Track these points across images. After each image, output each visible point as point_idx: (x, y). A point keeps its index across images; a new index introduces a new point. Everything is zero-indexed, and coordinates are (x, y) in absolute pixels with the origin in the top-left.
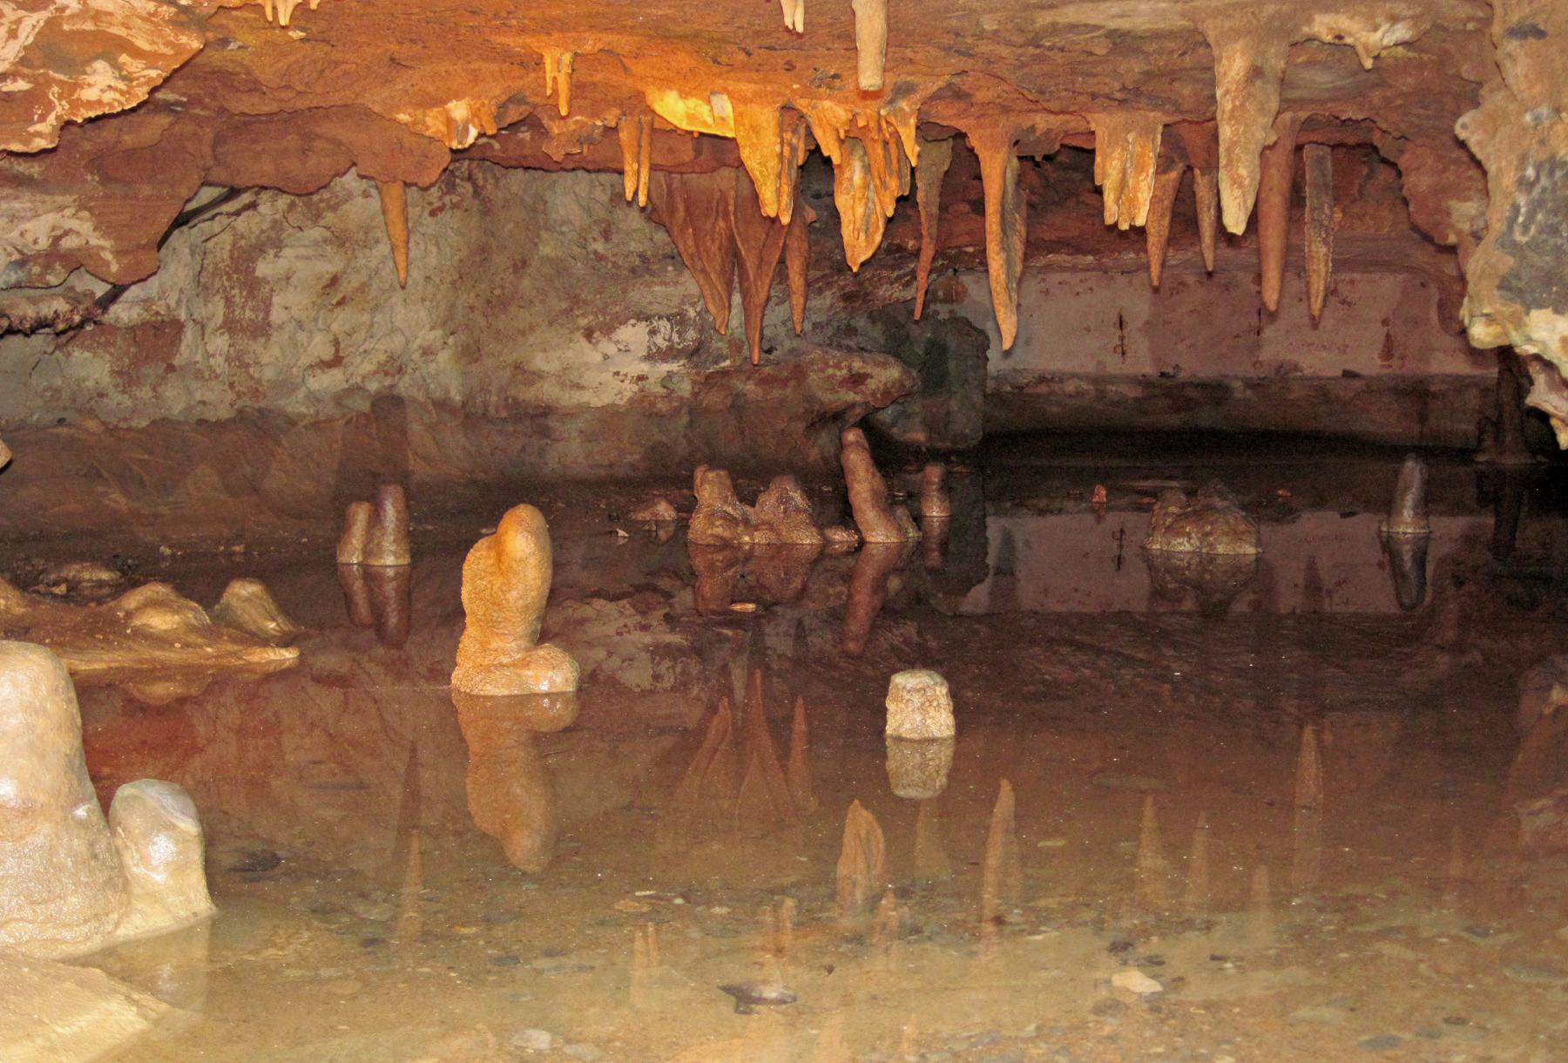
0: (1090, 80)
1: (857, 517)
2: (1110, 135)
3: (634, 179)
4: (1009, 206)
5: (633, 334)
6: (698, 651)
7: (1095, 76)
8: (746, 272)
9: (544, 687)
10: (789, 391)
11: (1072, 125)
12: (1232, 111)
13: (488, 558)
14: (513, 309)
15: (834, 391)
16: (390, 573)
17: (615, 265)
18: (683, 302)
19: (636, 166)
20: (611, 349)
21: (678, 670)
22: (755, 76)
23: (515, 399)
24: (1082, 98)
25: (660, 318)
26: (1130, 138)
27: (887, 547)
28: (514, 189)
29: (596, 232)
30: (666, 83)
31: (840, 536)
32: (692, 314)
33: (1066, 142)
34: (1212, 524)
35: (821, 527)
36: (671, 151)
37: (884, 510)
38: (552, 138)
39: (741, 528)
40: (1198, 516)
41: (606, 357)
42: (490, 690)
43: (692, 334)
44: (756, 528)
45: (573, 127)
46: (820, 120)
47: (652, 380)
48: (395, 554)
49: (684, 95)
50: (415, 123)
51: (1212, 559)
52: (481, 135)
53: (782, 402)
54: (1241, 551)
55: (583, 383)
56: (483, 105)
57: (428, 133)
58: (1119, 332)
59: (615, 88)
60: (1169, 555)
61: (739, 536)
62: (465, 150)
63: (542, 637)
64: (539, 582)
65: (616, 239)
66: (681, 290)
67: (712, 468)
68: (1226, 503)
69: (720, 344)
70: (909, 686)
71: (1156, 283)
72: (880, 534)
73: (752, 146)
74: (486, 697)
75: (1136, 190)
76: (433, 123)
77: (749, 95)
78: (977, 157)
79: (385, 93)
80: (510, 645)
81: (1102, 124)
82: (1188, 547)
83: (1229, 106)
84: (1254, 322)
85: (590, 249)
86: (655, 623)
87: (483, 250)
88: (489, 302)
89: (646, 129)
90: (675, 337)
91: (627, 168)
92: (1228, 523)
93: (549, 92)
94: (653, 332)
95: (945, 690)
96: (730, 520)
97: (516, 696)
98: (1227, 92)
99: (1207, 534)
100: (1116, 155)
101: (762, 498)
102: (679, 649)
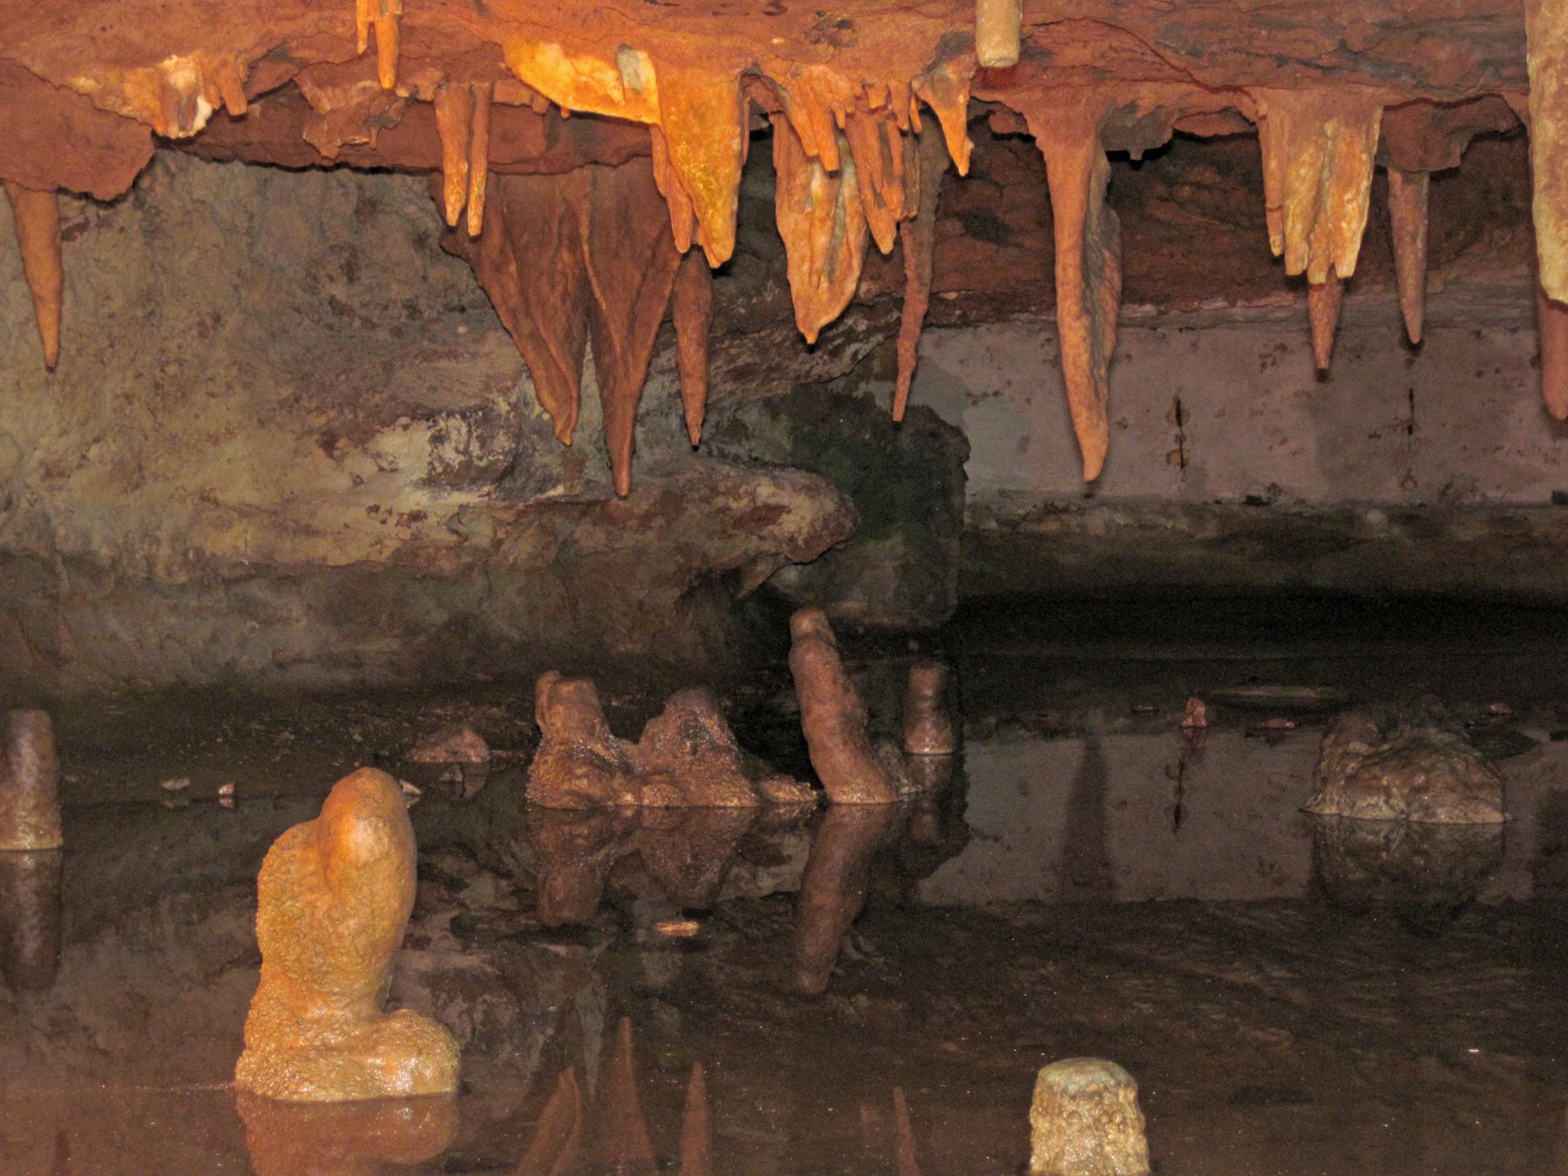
0: (1280, 36)
1: (817, 760)
2: (1295, 124)
3: (460, 189)
4: (1093, 238)
5: (406, 447)
6: (507, 982)
7: (1289, 27)
8: (608, 338)
9: (401, 1083)
10: (651, 535)
11: (1195, 100)
12: (1558, 95)
13: (305, 861)
14: (199, 397)
15: (725, 535)
16: (28, 861)
17: (366, 321)
18: (487, 387)
19: (464, 167)
20: (368, 468)
21: (478, 1016)
22: (709, 22)
23: (199, 551)
24: (1260, 65)
25: (450, 414)
26: (1329, 129)
27: (868, 811)
28: (198, 193)
29: (334, 264)
30: (543, 31)
31: (788, 793)
32: (503, 406)
33: (1186, 127)
34: (1427, 771)
35: (754, 778)
36: (506, 137)
37: (863, 748)
38: (322, 117)
39: (618, 781)
40: (1404, 757)
41: (358, 481)
42: (308, 1091)
43: (502, 442)
44: (645, 780)
45: (356, 100)
46: (802, 94)
47: (432, 520)
48: (36, 829)
49: (571, 51)
50: (106, 92)
51: (1428, 832)
52: (219, 113)
53: (640, 552)
54: (1478, 819)
55: (316, 523)
56: (224, 64)
57: (125, 111)
58: (1175, 430)
59: (449, 37)
60: (1353, 825)
61: (616, 795)
62: (188, 141)
63: (389, 1002)
64: (395, 904)
65: (366, 277)
66: (482, 366)
67: (568, 675)
68: (1448, 737)
69: (547, 459)
70: (1072, 1088)
71: (1323, 364)
72: (856, 791)
73: (693, 140)
74: (302, 1105)
75: (1339, 216)
76: (135, 94)
77: (690, 52)
78: (1040, 155)
79: (55, 41)
80: (334, 1014)
81: (1275, 110)
82: (1385, 812)
83: (1552, 87)
84: (1403, 411)
85: (324, 295)
86: (435, 935)
87: (148, 296)
88: (157, 386)
89: (481, 105)
90: (475, 448)
91: (449, 169)
92: (1453, 770)
93: (362, 47)
94: (438, 439)
95: (1132, 1095)
96: (601, 766)
97: (354, 1103)
98: (1549, 63)
99: (1418, 790)
100: (1305, 157)
101: (652, 727)
102: (476, 979)
